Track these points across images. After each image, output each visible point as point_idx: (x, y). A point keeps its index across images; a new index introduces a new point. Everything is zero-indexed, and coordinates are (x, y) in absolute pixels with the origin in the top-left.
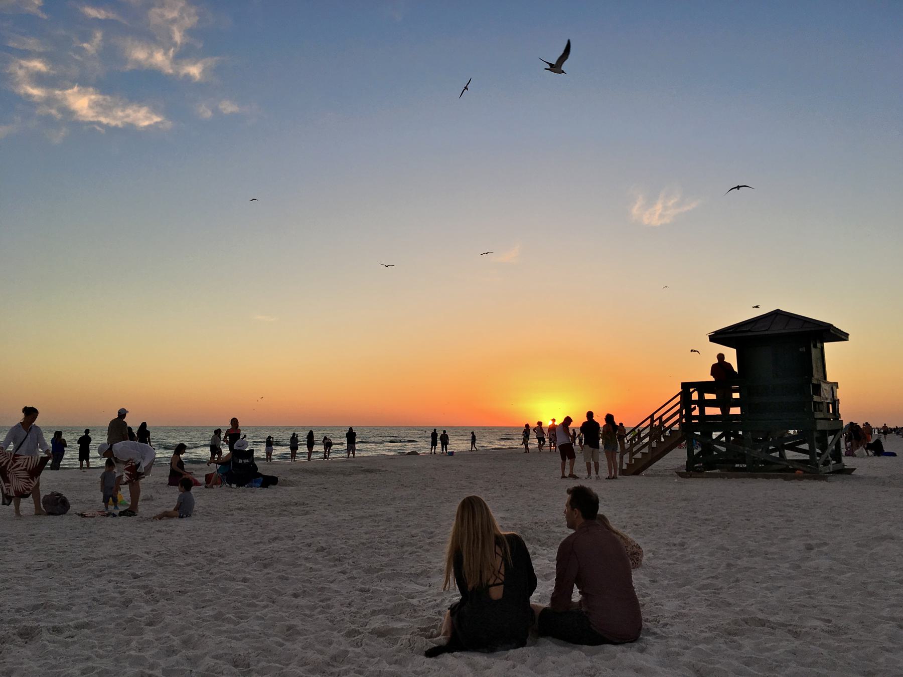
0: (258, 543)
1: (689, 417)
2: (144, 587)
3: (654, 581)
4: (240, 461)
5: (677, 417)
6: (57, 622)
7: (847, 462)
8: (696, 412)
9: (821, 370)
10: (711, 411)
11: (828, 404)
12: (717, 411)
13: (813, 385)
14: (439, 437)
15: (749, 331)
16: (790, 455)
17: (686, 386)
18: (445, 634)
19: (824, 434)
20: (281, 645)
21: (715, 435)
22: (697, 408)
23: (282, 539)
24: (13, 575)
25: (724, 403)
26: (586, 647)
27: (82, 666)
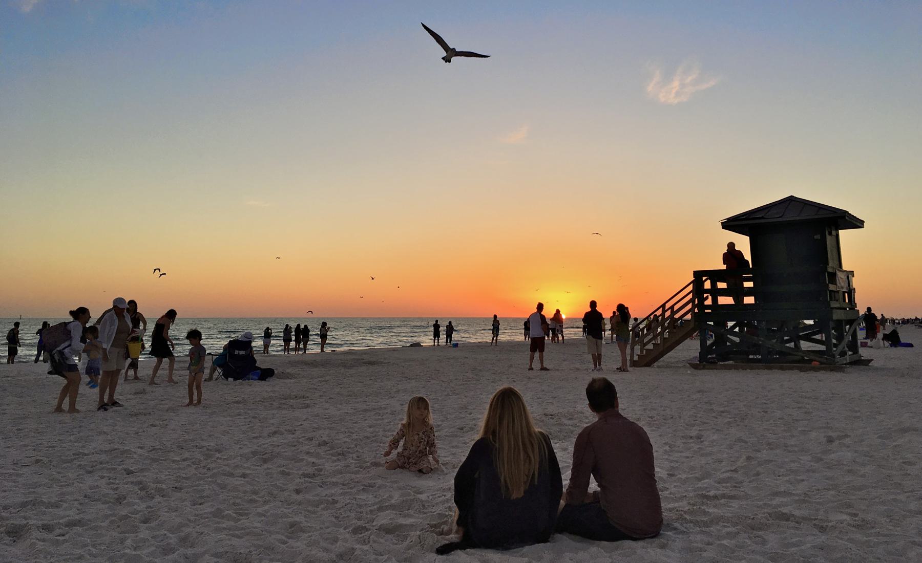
1: (701, 306)
5: (690, 306)
7: (864, 353)
8: (709, 302)
11: (844, 293)
13: (829, 273)
15: (762, 218)
16: (805, 345)
17: (698, 275)
18: (457, 532)
19: (839, 325)
20: (284, 543)
22: (710, 298)
25: (737, 292)
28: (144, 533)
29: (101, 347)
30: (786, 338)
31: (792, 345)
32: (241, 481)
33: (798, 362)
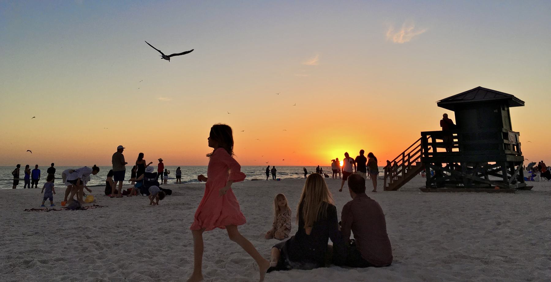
0: (161, 223)
1: (427, 153)
2: (95, 242)
3: (401, 239)
4: (149, 180)
5: (419, 154)
6: (44, 258)
7: (528, 184)
8: (431, 151)
9: (508, 124)
10: (440, 150)
11: (514, 145)
12: (444, 150)
13: (504, 133)
14: (271, 171)
15: (462, 100)
16: (491, 178)
17: (424, 134)
18: (274, 261)
19: (511, 164)
20: (178, 268)
21: (444, 165)
22: (432, 148)
23: (175, 221)
24: (15, 237)
25: (448, 145)
26: (359, 269)
27: (62, 276)
28: (99, 263)
29: (61, 189)
30: (479, 173)
31: (483, 177)
32: (153, 241)
33: (487, 187)
